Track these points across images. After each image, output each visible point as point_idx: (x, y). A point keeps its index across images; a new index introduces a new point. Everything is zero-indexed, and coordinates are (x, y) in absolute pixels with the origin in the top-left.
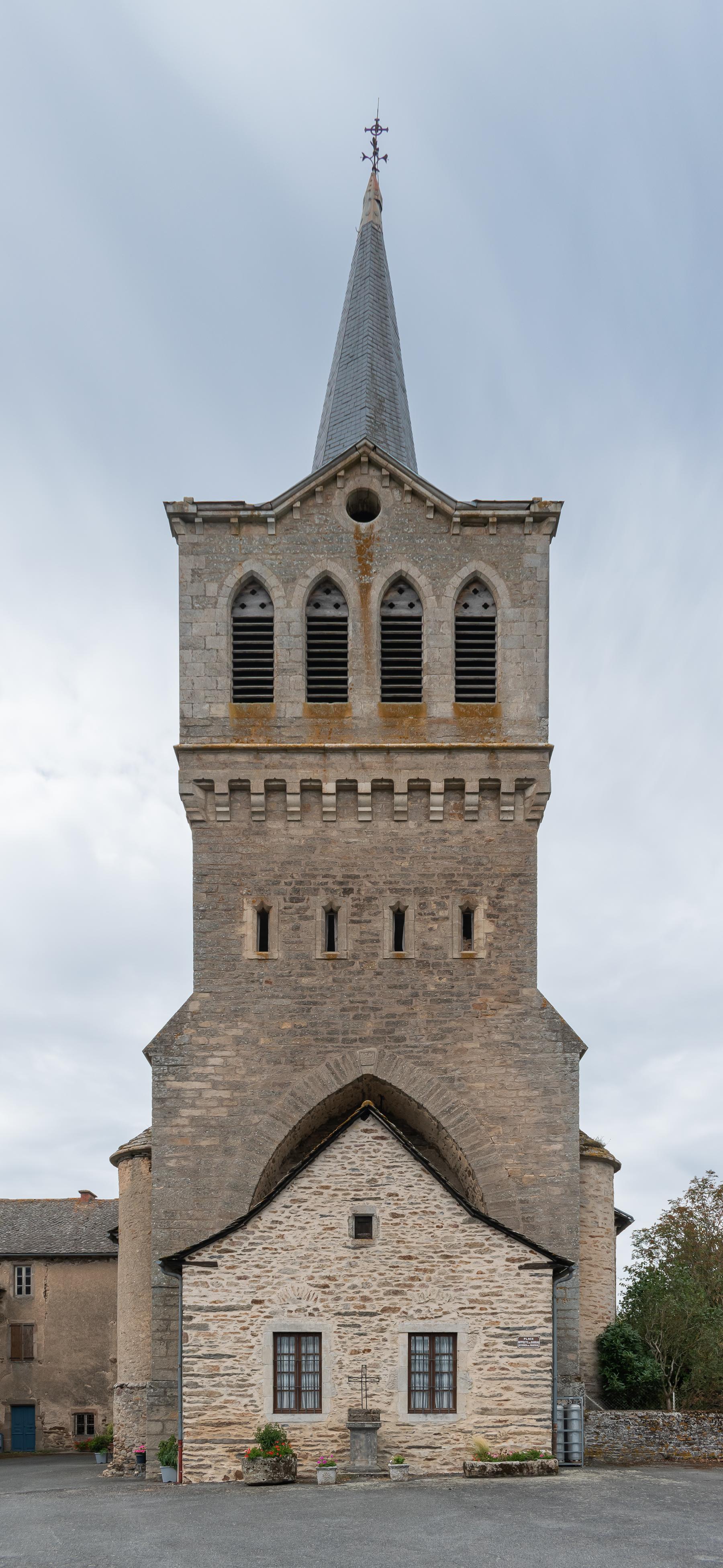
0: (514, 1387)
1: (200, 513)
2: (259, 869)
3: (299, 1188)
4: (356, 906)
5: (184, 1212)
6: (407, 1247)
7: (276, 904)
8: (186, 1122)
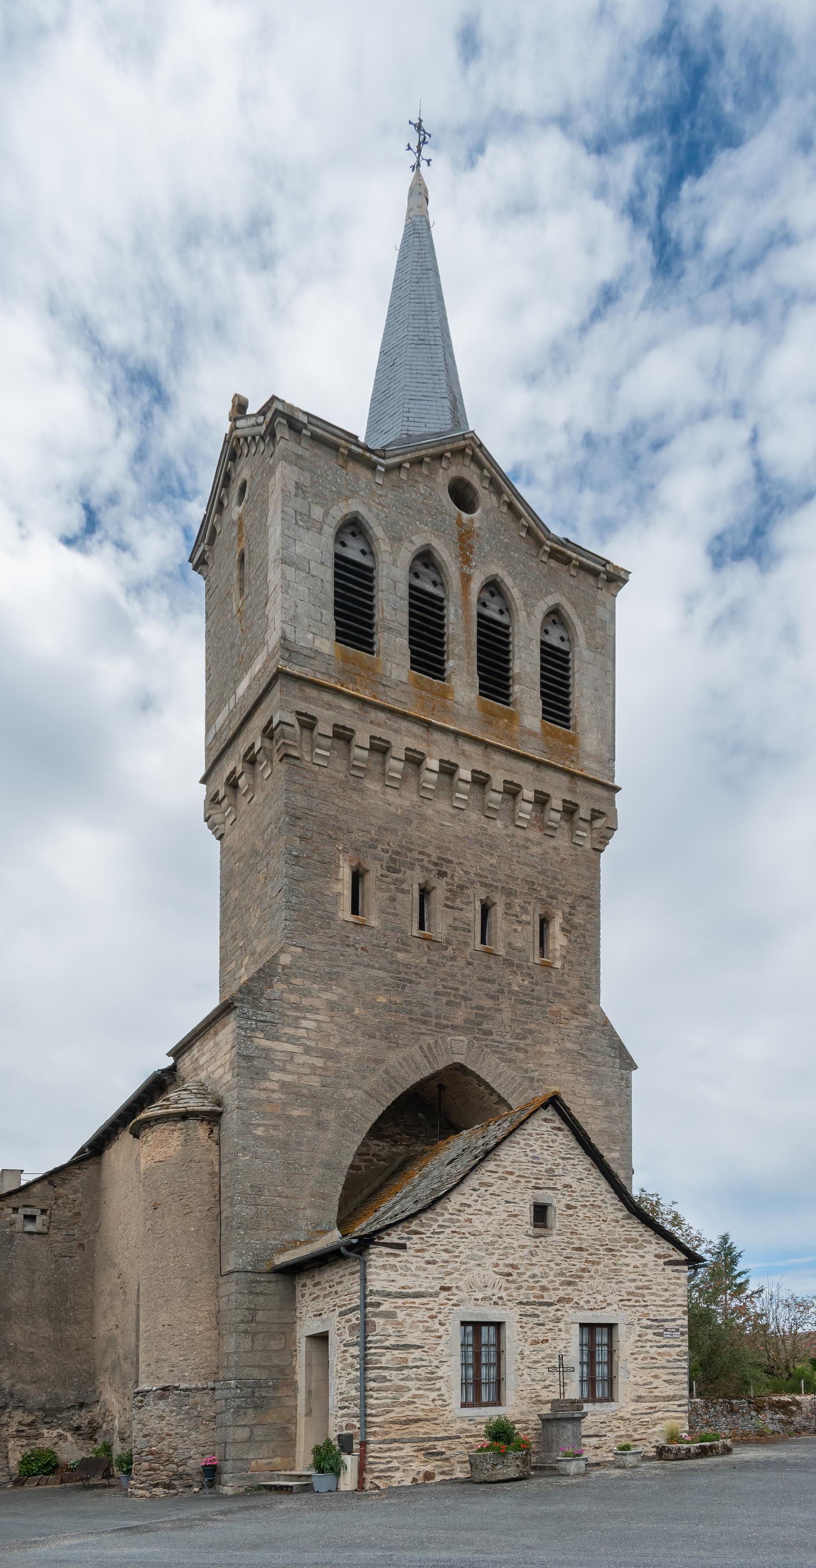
1: (310, 427)
2: (356, 827)
3: (487, 1171)
6: (579, 1239)
7: (374, 870)
8: (276, 1086)
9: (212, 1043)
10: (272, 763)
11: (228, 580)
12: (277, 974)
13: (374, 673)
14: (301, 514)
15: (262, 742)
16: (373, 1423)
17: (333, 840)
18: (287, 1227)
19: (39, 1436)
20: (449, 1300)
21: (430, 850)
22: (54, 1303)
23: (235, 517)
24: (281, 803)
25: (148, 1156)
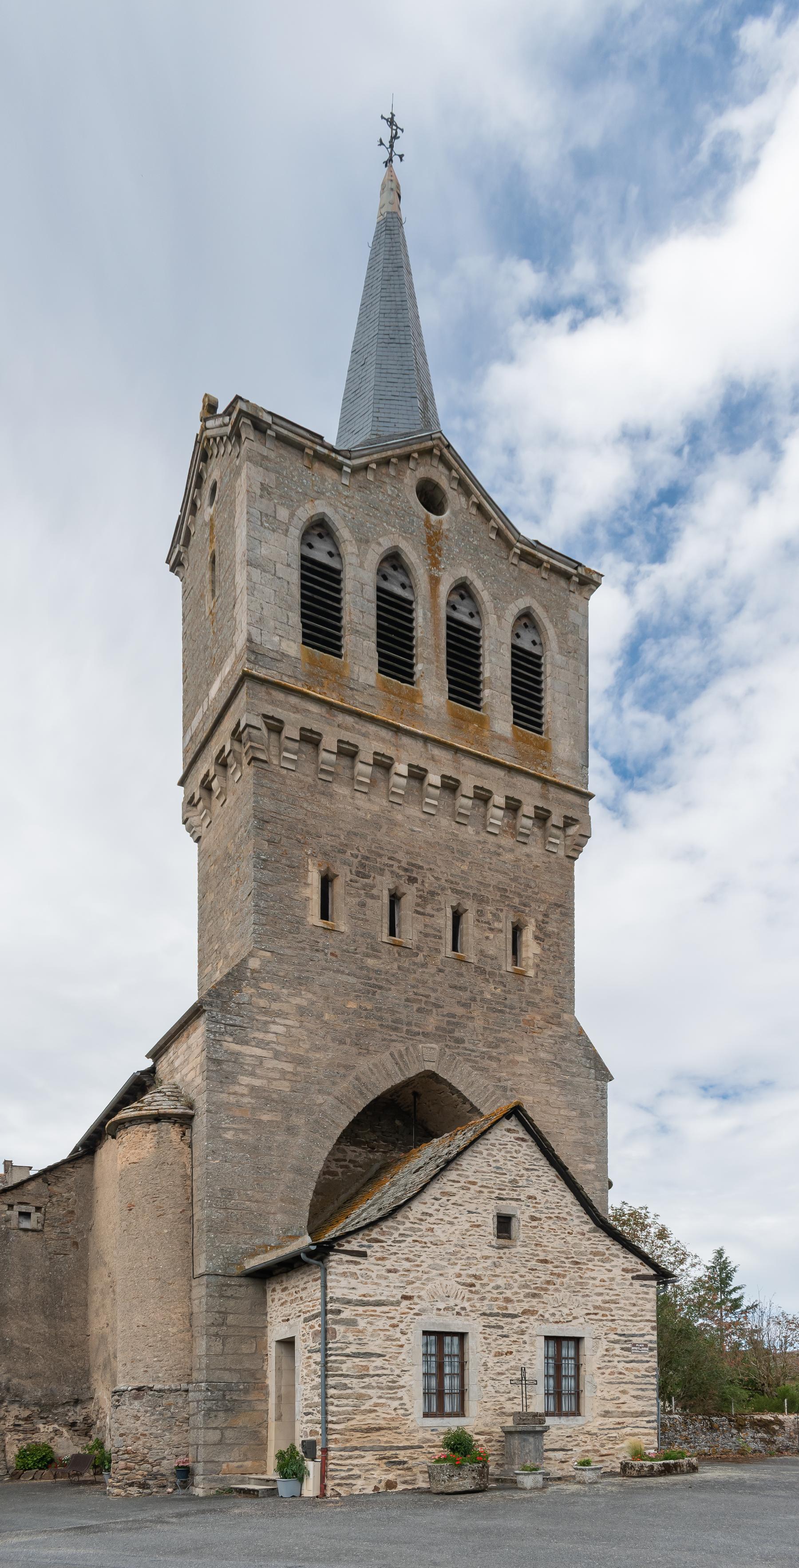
0: (629, 1390)
4: (421, 897)
5: (242, 1192)
6: (544, 1251)
8: (245, 1091)
9: (185, 1046)
10: (241, 766)
11: (201, 581)
12: (246, 978)
13: (342, 676)
14: (267, 515)
15: (232, 745)
16: (334, 1430)
17: (302, 844)
18: (258, 1231)
19: (35, 1431)
20: (411, 1309)
21: (400, 855)
22: (49, 1299)
23: (207, 519)
24: (250, 806)
25: (124, 1157)
